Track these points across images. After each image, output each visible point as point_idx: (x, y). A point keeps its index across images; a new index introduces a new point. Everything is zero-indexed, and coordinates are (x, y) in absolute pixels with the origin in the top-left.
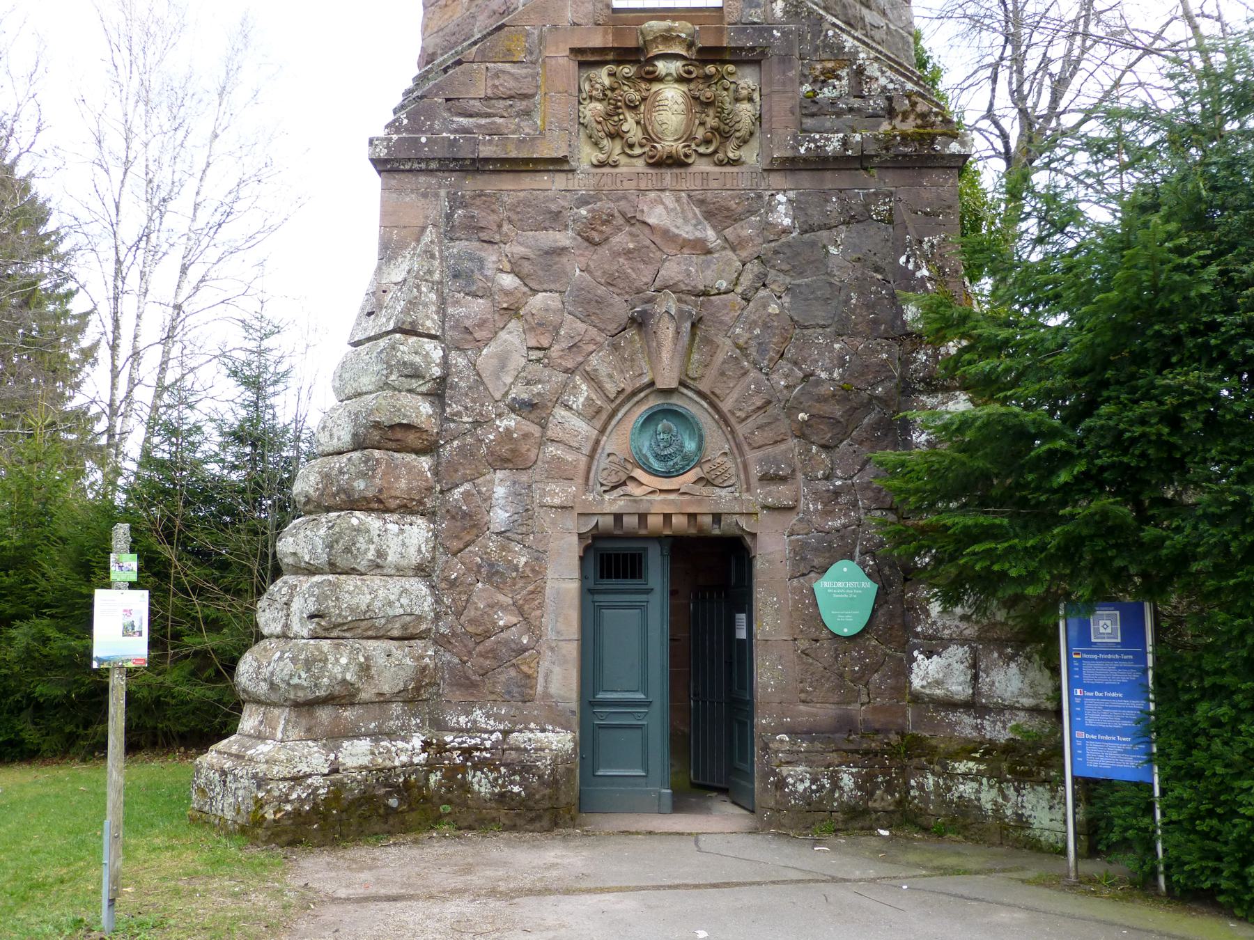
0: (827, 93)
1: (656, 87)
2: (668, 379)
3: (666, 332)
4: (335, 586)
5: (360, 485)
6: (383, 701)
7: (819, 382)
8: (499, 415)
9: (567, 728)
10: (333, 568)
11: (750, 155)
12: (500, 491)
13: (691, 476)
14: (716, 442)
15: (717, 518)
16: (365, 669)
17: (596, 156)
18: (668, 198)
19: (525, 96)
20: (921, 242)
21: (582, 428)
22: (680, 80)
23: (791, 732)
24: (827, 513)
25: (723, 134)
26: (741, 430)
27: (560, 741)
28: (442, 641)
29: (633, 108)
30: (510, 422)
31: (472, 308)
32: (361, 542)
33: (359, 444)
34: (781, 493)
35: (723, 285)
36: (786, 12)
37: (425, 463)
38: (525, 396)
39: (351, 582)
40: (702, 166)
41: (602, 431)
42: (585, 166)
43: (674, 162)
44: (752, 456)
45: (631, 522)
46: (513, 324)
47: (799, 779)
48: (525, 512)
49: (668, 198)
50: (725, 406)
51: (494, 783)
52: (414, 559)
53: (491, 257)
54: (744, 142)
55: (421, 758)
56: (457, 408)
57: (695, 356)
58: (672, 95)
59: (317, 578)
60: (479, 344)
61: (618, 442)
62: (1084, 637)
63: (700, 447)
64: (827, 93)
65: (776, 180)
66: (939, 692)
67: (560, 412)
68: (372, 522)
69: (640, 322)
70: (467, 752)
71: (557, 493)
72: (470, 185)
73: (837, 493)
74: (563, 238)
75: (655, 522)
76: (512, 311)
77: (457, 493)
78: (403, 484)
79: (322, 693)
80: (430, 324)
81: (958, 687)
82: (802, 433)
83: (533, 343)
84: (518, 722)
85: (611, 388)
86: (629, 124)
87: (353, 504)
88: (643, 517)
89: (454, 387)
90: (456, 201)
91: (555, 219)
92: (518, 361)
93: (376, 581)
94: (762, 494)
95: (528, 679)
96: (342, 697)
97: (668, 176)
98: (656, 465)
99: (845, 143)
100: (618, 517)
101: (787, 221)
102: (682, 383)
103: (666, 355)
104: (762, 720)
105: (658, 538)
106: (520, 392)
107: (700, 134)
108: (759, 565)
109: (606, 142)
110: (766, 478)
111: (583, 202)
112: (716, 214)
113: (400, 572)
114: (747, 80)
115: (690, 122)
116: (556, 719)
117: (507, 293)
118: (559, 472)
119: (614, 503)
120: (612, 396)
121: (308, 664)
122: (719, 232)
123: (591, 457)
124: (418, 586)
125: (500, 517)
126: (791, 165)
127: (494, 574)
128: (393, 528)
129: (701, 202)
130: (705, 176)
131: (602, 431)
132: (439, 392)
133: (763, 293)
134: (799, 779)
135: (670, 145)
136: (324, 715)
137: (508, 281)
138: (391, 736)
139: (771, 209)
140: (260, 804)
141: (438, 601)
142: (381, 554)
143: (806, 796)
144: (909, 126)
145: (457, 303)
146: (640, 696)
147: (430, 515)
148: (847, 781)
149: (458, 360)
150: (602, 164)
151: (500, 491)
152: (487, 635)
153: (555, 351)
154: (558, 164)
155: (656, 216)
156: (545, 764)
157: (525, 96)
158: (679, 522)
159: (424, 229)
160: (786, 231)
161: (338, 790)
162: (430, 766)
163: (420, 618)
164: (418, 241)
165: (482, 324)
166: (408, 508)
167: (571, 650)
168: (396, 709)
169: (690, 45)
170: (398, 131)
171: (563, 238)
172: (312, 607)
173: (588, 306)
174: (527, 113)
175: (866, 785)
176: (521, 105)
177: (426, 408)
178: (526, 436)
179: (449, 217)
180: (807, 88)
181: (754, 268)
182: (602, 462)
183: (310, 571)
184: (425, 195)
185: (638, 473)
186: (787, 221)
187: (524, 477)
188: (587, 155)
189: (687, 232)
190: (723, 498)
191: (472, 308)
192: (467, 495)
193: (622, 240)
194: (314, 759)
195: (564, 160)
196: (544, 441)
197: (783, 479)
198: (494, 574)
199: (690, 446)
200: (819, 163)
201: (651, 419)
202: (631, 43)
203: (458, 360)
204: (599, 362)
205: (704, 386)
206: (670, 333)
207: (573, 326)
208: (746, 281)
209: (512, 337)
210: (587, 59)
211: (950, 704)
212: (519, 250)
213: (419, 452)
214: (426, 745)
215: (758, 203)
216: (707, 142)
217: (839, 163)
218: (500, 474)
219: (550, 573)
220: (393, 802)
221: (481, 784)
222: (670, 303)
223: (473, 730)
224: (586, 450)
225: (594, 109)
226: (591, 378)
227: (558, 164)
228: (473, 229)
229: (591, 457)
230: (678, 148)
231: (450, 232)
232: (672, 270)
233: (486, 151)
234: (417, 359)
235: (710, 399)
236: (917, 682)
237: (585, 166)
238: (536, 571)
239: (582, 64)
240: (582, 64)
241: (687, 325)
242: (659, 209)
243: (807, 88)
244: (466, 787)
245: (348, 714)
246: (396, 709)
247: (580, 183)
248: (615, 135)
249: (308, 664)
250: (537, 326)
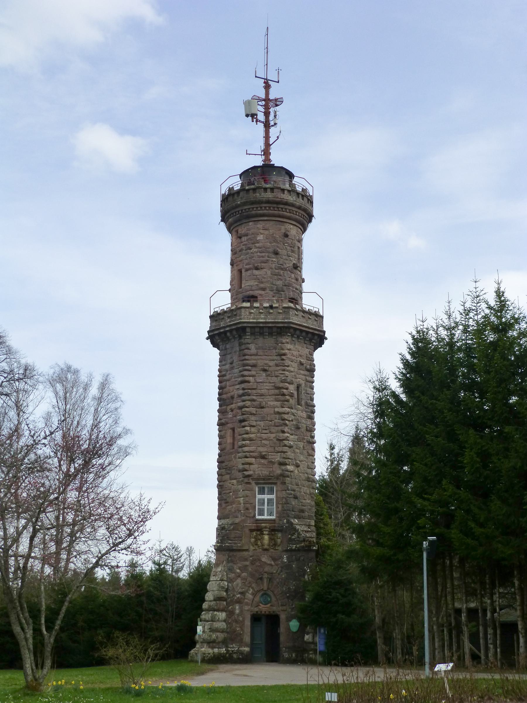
0: (293, 537)
1: (264, 536)
2: (265, 588)
3: (265, 580)
4: (213, 624)
5: (216, 607)
6: (219, 643)
7: (291, 589)
8: (237, 594)
9: (249, 647)
10: (212, 621)
11: (280, 548)
12: (237, 607)
13: (269, 605)
14: (274, 599)
15: (274, 612)
16: (217, 637)
17: (253, 548)
18: (265, 556)
19: (241, 537)
20: (308, 565)
21: (251, 597)
22: (268, 535)
23: (286, 648)
24: (292, 611)
25: (275, 545)
26: (278, 597)
27: (247, 649)
28: (228, 633)
29: (260, 540)
30: (239, 596)
31: (232, 575)
32: (216, 617)
33: (215, 600)
34: (284, 608)
35: (275, 572)
36: (286, 522)
37: (225, 603)
38: (241, 591)
39: (214, 623)
40: (272, 550)
41: (254, 597)
42: (251, 550)
43: (266, 550)
44: (280, 602)
45: (259, 613)
46: (239, 579)
47: (286, 655)
48: (241, 611)
49: (265, 556)
50: (275, 593)
51: (237, 656)
52: (223, 619)
53: (235, 566)
54: (279, 546)
55: (225, 652)
56: (230, 593)
57: (270, 584)
58: (266, 537)
59: (209, 623)
60: (233, 582)
61: (257, 599)
62: (320, 632)
63: (271, 599)
64: (293, 537)
65: (284, 553)
66: (308, 641)
67: (247, 594)
68: (218, 613)
69: (261, 579)
70: (232, 651)
71: (246, 608)
72: (231, 554)
73: (293, 608)
74: (247, 563)
75: (263, 612)
76: (239, 576)
77: (230, 607)
78: (222, 607)
79: (211, 641)
80: (225, 579)
81: (311, 640)
82: (288, 597)
83: (243, 582)
84: (241, 646)
85: (256, 590)
86: (259, 543)
87: (214, 610)
88: (261, 612)
89: (229, 589)
90: (229, 557)
91: (246, 560)
92: (240, 585)
93: (218, 623)
94: (281, 608)
95: (242, 639)
96: (214, 641)
97: (266, 552)
98: (263, 603)
99: (296, 547)
100: (257, 612)
101: (286, 561)
102: (268, 589)
103: (265, 585)
104: (281, 646)
105: (264, 615)
106: (240, 590)
107: (271, 544)
108: (281, 620)
109: (255, 546)
110: (282, 605)
111: (251, 557)
112: (274, 559)
113: (221, 621)
114: (280, 535)
115: (269, 542)
116: (246, 645)
117: (238, 573)
118: (247, 604)
119: (256, 609)
120: (279, 263)
121: (210, 636)
122: (274, 562)
123: (252, 601)
124: (224, 624)
125: (237, 611)
126: (287, 551)
127: (236, 621)
128: (220, 614)
129: (271, 557)
130: (272, 552)
131: (254, 597)
132: (227, 591)
133: (281, 573)
134: (286, 655)
135: (266, 547)
136: (211, 644)
137: (238, 571)
138: (220, 648)
139: (283, 558)
140: (204, 657)
141: (227, 626)
142: (219, 618)
143: (287, 658)
144: (307, 543)
145: (229, 575)
146: (261, 642)
147: (226, 611)
148: (294, 655)
149: (230, 585)
150: (254, 550)
151: (237, 607)
152: (235, 632)
153: (246, 583)
154: (247, 550)
155: (263, 560)
156: (245, 652)
157: (241, 537)
158: (267, 613)
159: (223, 561)
160: (286, 562)
161: (214, 656)
162: (227, 653)
163: (225, 629)
164: (223, 563)
165: (234, 578)
166: (222, 610)
167: (249, 634)
168: (221, 644)
169: (269, 528)
170: (218, 543)
171: (247, 563)
172: (209, 627)
173: (252, 575)
174: (241, 540)
175: (297, 656)
176: (240, 539)
177: (225, 594)
178: (242, 598)
179: (228, 559)
180: (290, 536)
181: (280, 569)
182: (254, 602)
183: (208, 621)
184: (224, 555)
185: (261, 604)
186: (286, 561)
187: (241, 605)
188: (252, 548)
189: (269, 562)
190: (274, 608)
191: (232, 575)
192: (232, 608)
193: (258, 564)
194: (210, 651)
195: (248, 549)
196: (245, 599)
197: (284, 606)
198: (236, 621)
199: (269, 599)
200: (291, 550)
201: (263, 595)
202: (259, 528)
203: (230, 585)
204: (254, 585)
205: (271, 589)
206: (266, 580)
207: (249, 579)
208: (279, 571)
209: (239, 581)
210: (251, 531)
211: (310, 643)
212: (240, 565)
213: (224, 601)
214: (226, 650)
215: (281, 557)
216: (272, 546)
217: (294, 550)
218: (237, 604)
219: (246, 621)
220: (222, 658)
221: (235, 656)
222: (266, 576)
223: (233, 648)
224: (251, 600)
225: (253, 540)
226: (253, 588)
227: (247, 550)
228: (232, 561)
229: (252, 601)
230: (268, 547)
231: (228, 562)
232: (267, 569)
233: (234, 548)
234: (224, 585)
235: (273, 592)
236: (305, 639)
237: (251, 550)
238: (243, 621)
239: (251, 531)
240: (251, 531)
241: (268, 580)
242: (264, 558)
243: (290, 536)
244: (232, 657)
245: (214, 644)
246: (221, 644)
247: (250, 553)
248: (256, 544)
249: (210, 636)
250: (244, 579)
